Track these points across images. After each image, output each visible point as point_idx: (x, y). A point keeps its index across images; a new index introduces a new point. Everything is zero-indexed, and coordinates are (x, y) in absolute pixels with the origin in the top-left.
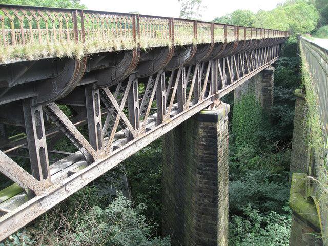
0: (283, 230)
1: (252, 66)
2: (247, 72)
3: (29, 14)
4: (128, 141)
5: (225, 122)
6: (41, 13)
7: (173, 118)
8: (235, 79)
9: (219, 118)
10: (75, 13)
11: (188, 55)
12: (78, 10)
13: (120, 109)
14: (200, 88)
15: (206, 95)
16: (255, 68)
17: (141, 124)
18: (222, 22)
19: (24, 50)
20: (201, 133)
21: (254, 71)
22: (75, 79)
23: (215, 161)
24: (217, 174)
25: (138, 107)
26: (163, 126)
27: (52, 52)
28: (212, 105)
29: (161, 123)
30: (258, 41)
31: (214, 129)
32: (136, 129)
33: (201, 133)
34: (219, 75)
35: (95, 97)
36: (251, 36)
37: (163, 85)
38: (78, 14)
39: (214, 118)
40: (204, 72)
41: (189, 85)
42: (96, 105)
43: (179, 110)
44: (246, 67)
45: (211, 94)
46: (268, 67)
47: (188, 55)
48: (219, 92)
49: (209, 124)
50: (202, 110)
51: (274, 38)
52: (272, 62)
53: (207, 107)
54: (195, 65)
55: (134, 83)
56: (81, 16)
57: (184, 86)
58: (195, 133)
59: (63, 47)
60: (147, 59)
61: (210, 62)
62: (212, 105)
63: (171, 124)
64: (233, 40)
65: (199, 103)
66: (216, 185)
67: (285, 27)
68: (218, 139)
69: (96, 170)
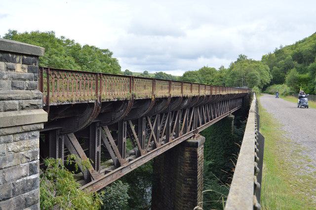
0: (273, 108)
2: (215, 118)
3: (58, 74)
4: (153, 149)
6: (60, 73)
7: (163, 146)
9: (199, 145)
11: (187, 102)
12: (45, 68)
13: (152, 129)
14: (187, 124)
15: (191, 130)
16: (220, 115)
18: (168, 79)
19: (191, 92)
20: (187, 155)
22: (89, 118)
23: (196, 174)
24: (197, 184)
26: (169, 144)
28: (194, 136)
30: (224, 96)
31: (196, 153)
33: (187, 155)
36: (191, 92)
37: (125, 132)
38: (99, 75)
39: (196, 145)
40: (174, 120)
42: (144, 126)
44: (214, 114)
47: (186, 103)
49: (192, 148)
50: (188, 139)
52: (233, 111)
53: (191, 138)
54: (186, 109)
57: (180, 121)
58: (183, 155)
59: (87, 96)
61: (194, 108)
62: (194, 136)
63: (172, 144)
64: (209, 94)
65: (187, 134)
66: (196, 192)
67: (142, 72)
69: (141, 161)
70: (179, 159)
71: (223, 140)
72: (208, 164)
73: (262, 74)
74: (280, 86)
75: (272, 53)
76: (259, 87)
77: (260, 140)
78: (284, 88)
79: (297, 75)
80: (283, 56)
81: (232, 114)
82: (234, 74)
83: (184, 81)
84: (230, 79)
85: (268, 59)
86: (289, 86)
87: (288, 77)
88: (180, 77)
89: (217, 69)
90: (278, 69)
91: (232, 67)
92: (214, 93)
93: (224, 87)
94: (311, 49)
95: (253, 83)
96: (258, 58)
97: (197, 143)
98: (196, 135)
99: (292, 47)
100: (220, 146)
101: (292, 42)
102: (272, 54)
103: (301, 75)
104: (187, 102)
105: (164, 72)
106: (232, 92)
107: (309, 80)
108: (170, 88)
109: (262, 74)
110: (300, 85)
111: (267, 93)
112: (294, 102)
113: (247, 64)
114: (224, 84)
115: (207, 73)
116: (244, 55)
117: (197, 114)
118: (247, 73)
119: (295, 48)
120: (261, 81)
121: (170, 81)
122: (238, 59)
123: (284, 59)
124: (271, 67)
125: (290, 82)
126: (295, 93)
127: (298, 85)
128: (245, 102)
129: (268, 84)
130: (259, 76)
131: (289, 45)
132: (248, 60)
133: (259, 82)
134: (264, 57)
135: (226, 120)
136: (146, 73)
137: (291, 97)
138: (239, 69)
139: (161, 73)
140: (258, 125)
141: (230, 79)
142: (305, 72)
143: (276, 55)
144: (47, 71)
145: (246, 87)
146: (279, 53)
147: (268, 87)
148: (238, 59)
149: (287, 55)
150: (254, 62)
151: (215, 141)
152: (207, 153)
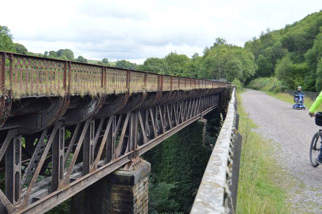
0: (264, 116)
1: (181, 118)
2: (175, 125)
5: (144, 185)
8: (161, 132)
9: (136, 181)
10: (4, 56)
11: (93, 106)
12: (7, 54)
15: (123, 153)
16: (185, 120)
17: (24, 192)
20: (116, 197)
21: (183, 123)
25: (63, 155)
26: (57, 195)
27: (44, 92)
29: (56, 190)
30: (188, 92)
32: (14, 201)
33: (116, 197)
34: (140, 131)
35: (16, 144)
39: (130, 181)
41: (120, 132)
43: (84, 171)
44: (173, 119)
45: (129, 151)
46: (200, 119)
47: (92, 109)
48: (139, 147)
49: (123, 186)
50: (117, 170)
51: (207, 89)
52: (205, 113)
53: (123, 166)
55: (15, 141)
56: (11, 60)
57: (114, 135)
58: (109, 198)
60: (33, 110)
64: (155, 89)
67: (101, 60)
68: (134, 206)
70: (103, 204)
71: (190, 155)
72: (169, 189)
73: (244, 63)
74: (267, 79)
75: (258, 38)
76: (241, 81)
77: (237, 144)
78: (274, 81)
79: (290, 64)
80: (271, 41)
81: (204, 117)
82: (208, 62)
83: (147, 70)
84: (204, 69)
85: (252, 46)
86: (280, 79)
87: (279, 67)
88: (141, 66)
89: (190, 57)
90: (263, 57)
91: (207, 53)
92: (214, 87)
93: (195, 79)
94: (304, 33)
95: (233, 75)
96: (242, 45)
97: (132, 178)
98: (134, 160)
99: (281, 32)
100: (187, 163)
101: (281, 26)
102: (257, 40)
103: (295, 65)
104: (93, 106)
105: (127, 60)
106: (203, 86)
107: (306, 72)
108: (128, 81)
109: (244, 63)
110: (294, 79)
111: (251, 88)
112: (287, 101)
113: (225, 49)
114: (196, 76)
115: (176, 62)
116: (222, 39)
117: (134, 123)
118: (226, 61)
119: (285, 32)
120: (244, 72)
121: (124, 69)
122: (215, 44)
123: (271, 45)
124: (256, 55)
125: (281, 73)
126: (291, 88)
127: (291, 78)
128: (222, 98)
129: (251, 76)
130: (240, 66)
131: (276, 29)
132: (227, 46)
133: (241, 73)
134: (247, 44)
135: (195, 126)
136: (105, 61)
137: (284, 95)
138: (215, 56)
139: (124, 61)
140: (236, 108)
141: (204, 69)
142: (302, 59)
143: (262, 40)
144: (10, 57)
145: (225, 81)
146: (266, 38)
147: (252, 81)
148: (215, 44)
149: (275, 41)
150: (236, 47)
151: (180, 154)
152: (169, 172)
